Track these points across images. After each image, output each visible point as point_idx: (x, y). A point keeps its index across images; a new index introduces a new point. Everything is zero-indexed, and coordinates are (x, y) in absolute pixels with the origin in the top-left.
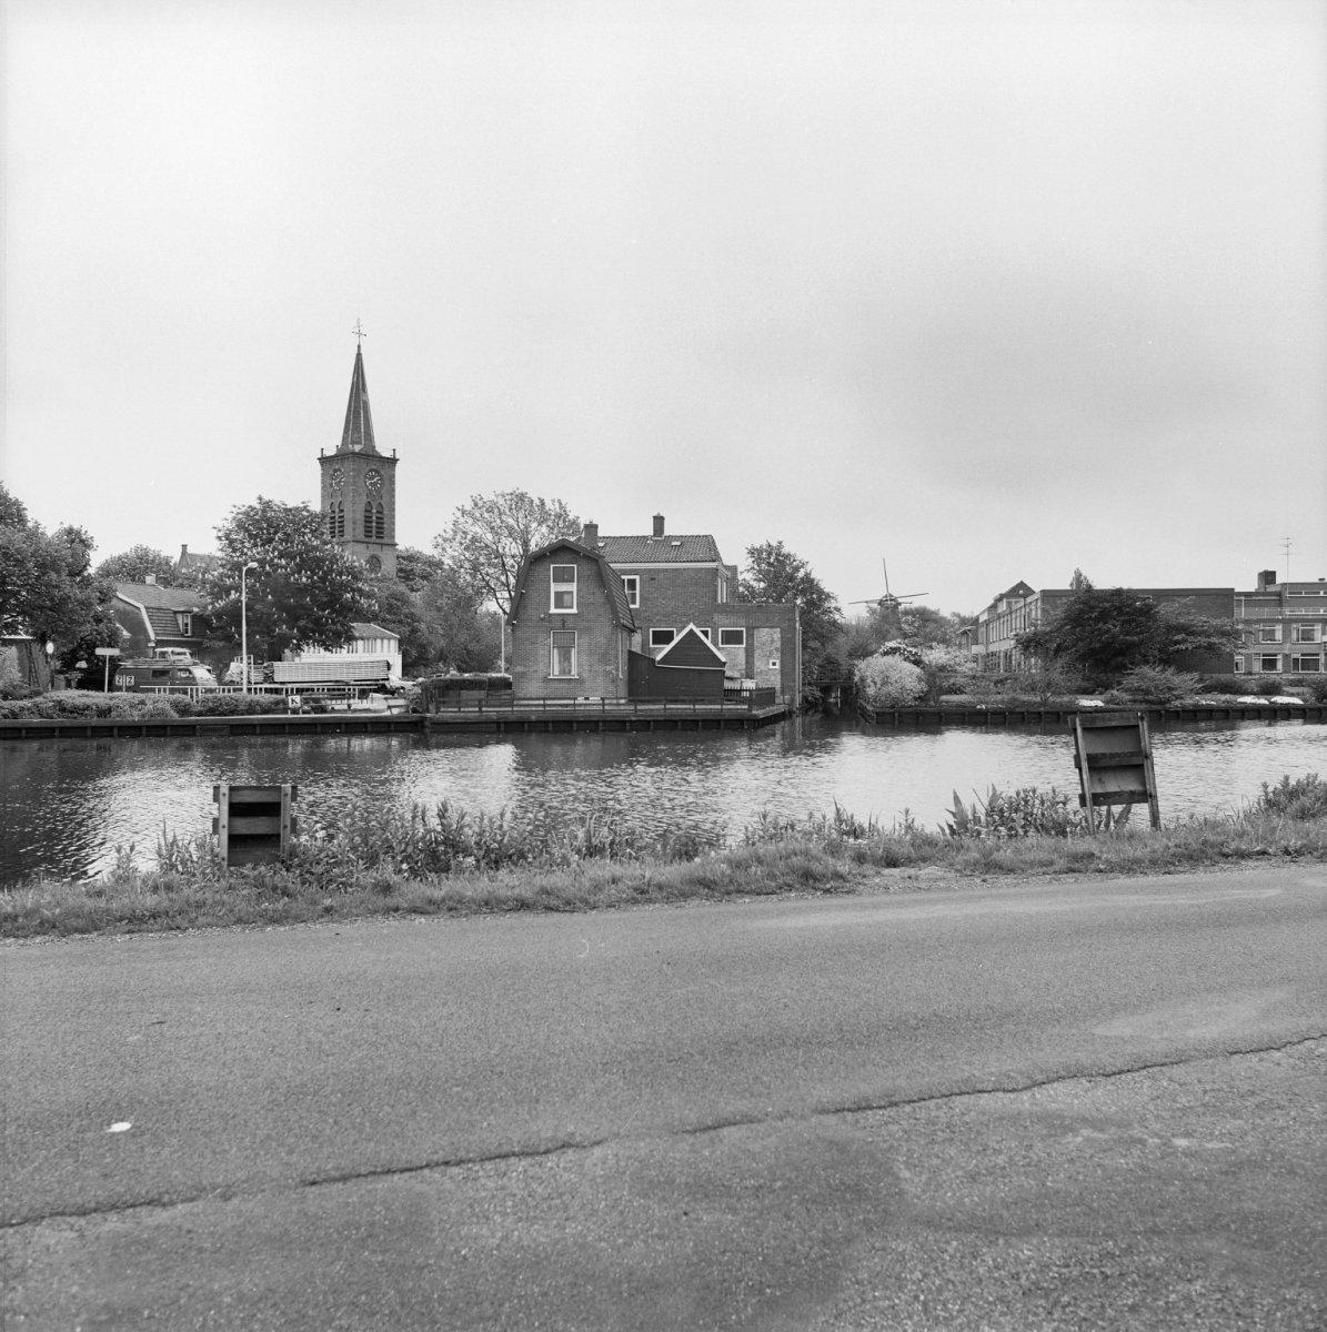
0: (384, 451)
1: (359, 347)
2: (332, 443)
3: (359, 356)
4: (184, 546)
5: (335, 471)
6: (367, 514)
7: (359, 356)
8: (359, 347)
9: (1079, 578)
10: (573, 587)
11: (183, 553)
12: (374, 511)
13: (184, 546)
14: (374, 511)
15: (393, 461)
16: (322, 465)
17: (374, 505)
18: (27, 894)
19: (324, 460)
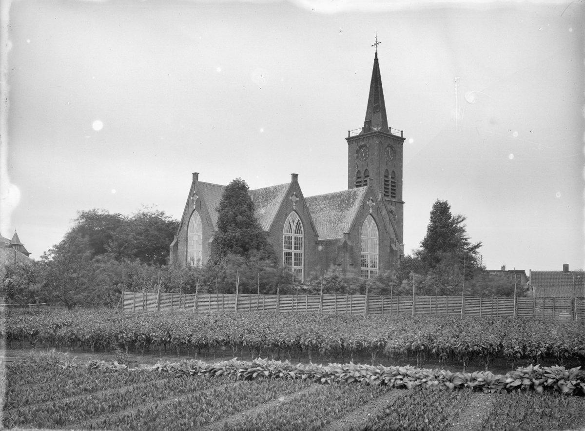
0: (395, 132)
1: (376, 54)
2: (357, 128)
3: (376, 60)
4: (196, 175)
5: (361, 147)
6: (394, 193)
7: (376, 60)
8: (376, 54)
9: (16, 236)
10: (302, 251)
11: (194, 183)
12: (390, 177)
13: (196, 175)
14: (390, 177)
15: (401, 140)
16: (349, 143)
17: (390, 172)
18: (361, 280)
19: (350, 140)
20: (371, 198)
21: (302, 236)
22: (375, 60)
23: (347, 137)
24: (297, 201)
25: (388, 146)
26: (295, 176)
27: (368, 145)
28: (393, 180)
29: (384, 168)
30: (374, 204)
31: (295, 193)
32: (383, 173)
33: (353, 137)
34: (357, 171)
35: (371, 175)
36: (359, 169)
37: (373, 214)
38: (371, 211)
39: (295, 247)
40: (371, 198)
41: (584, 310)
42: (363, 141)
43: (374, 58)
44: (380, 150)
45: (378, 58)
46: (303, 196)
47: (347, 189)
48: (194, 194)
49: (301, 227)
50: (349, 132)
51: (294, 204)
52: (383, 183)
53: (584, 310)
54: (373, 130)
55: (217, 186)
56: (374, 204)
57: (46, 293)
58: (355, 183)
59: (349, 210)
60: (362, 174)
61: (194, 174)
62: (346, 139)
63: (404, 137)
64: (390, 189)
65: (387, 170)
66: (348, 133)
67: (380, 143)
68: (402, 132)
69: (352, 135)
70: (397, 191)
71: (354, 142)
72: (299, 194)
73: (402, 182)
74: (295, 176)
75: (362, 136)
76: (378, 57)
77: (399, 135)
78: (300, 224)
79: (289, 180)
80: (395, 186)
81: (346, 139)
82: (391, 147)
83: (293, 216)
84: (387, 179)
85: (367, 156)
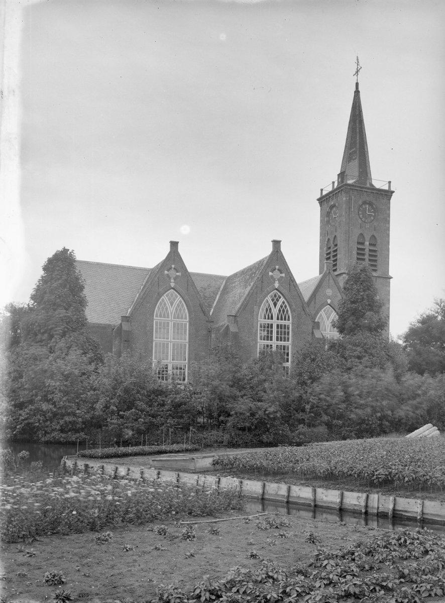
1: (357, 84)
3: (357, 92)
5: (332, 207)
7: (357, 92)
8: (357, 84)
10: (288, 344)
12: (367, 243)
14: (367, 243)
20: (277, 267)
21: (289, 323)
22: (355, 92)
24: (177, 276)
25: (365, 203)
28: (372, 248)
29: (357, 232)
30: (283, 275)
31: (173, 266)
32: (355, 238)
33: (327, 195)
37: (281, 289)
38: (277, 285)
39: (277, 337)
40: (277, 267)
41: (434, 508)
43: (354, 89)
44: (350, 208)
45: (360, 89)
46: (186, 270)
49: (287, 311)
50: (322, 190)
51: (172, 281)
52: (355, 252)
53: (434, 508)
55: (98, 264)
56: (283, 275)
57: (38, 398)
58: (325, 255)
63: (392, 189)
64: (367, 260)
65: (361, 234)
66: (320, 191)
67: (350, 199)
68: (390, 182)
70: (379, 263)
72: (181, 266)
73: (388, 250)
74: (277, 244)
76: (360, 89)
77: (386, 188)
78: (286, 307)
80: (376, 256)
81: (318, 200)
82: (370, 204)
83: (172, 296)
84: (363, 247)
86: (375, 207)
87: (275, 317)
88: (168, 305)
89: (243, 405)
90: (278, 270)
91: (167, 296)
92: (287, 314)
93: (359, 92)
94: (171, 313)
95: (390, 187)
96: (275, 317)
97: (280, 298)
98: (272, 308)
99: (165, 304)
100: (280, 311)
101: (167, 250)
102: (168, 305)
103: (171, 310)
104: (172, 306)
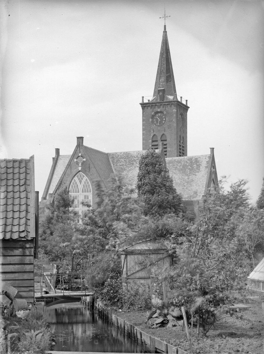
1: (165, 26)
2: (149, 96)
3: (165, 32)
5: (157, 113)
7: (165, 32)
8: (165, 26)
19: (144, 106)
22: (164, 32)
23: (141, 102)
26: (212, 149)
27: (165, 113)
34: (152, 135)
35: (168, 139)
36: (155, 133)
42: (159, 107)
43: (163, 30)
45: (167, 30)
47: (141, 149)
48: (79, 156)
50: (143, 97)
54: (167, 98)
58: (151, 146)
59: (196, 175)
60: (159, 138)
61: (78, 138)
62: (141, 104)
63: (188, 105)
66: (141, 98)
69: (146, 101)
71: (149, 108)
74: (212, 149)
75: (154, 103)
79: (209, 153)
85: (164, 122)
86: (183, 117)
87: (81, 191)
88: (78, 183)
89: (245, 246)
90: (81, 156)
91: (77, 177)
92: (89, 188)
93: (166, 32)
94: (80, 189)
95: (187, 103)
96: (81, 191)
97: (84, 176)
98: (78, 185)
99: (76, 183)
100: (84, 186)
101: (75, 144)
102: (78, 183)
103: (81, 187)
104: (80, 184)
